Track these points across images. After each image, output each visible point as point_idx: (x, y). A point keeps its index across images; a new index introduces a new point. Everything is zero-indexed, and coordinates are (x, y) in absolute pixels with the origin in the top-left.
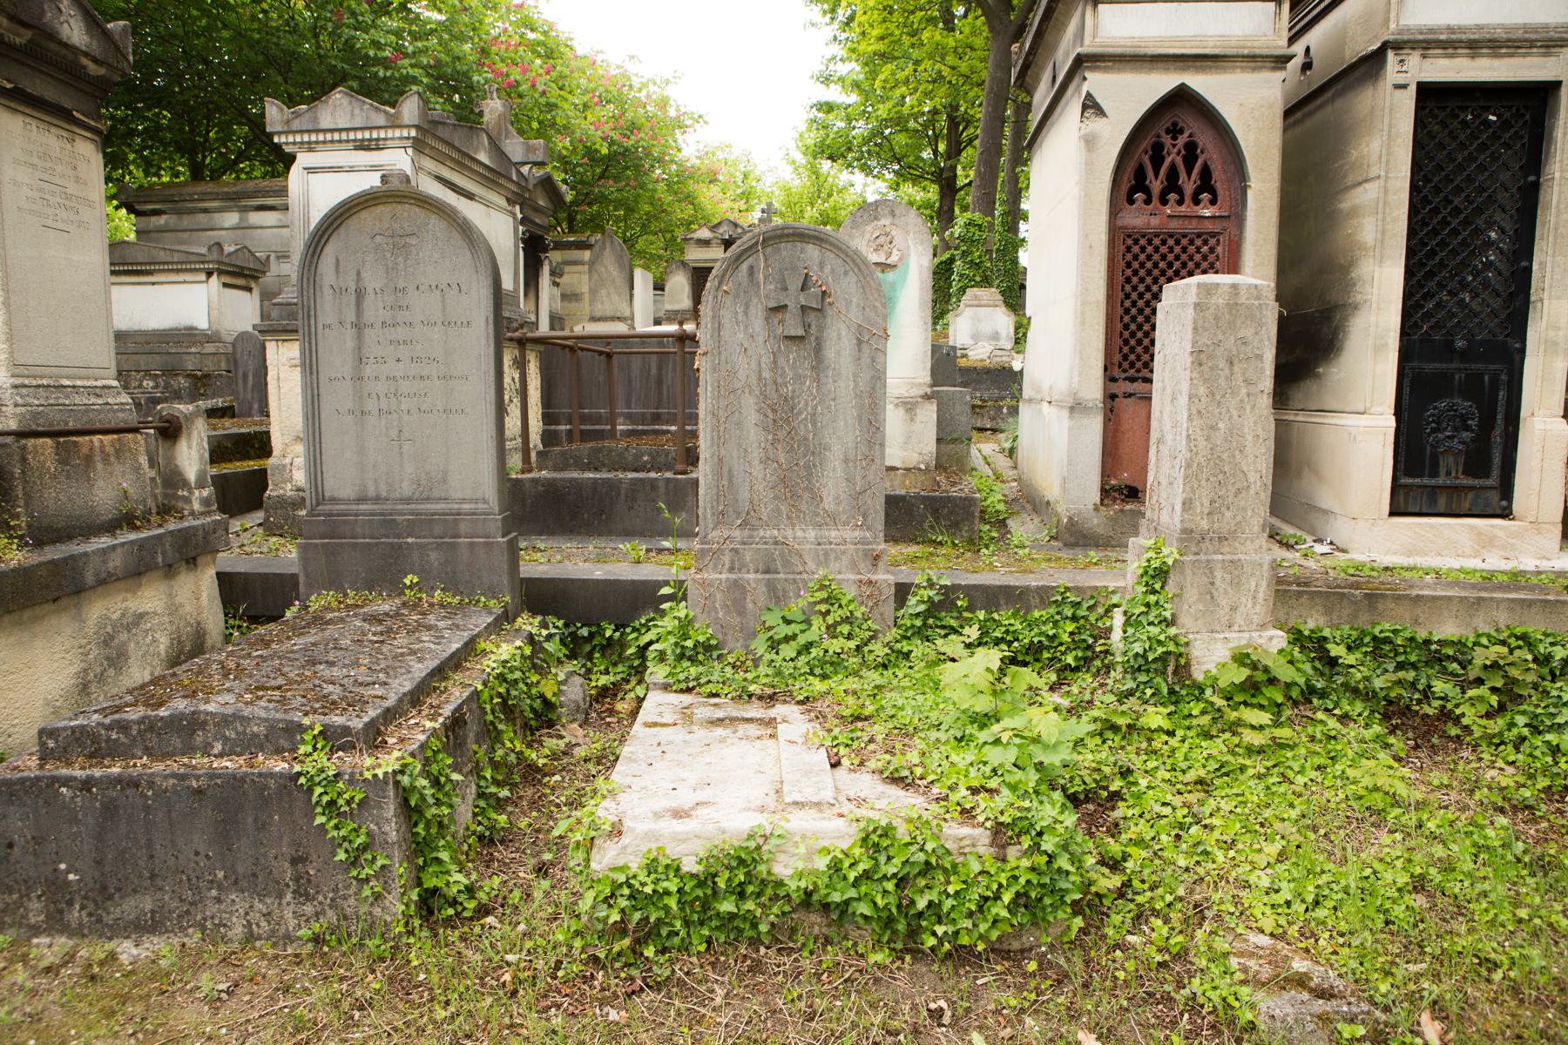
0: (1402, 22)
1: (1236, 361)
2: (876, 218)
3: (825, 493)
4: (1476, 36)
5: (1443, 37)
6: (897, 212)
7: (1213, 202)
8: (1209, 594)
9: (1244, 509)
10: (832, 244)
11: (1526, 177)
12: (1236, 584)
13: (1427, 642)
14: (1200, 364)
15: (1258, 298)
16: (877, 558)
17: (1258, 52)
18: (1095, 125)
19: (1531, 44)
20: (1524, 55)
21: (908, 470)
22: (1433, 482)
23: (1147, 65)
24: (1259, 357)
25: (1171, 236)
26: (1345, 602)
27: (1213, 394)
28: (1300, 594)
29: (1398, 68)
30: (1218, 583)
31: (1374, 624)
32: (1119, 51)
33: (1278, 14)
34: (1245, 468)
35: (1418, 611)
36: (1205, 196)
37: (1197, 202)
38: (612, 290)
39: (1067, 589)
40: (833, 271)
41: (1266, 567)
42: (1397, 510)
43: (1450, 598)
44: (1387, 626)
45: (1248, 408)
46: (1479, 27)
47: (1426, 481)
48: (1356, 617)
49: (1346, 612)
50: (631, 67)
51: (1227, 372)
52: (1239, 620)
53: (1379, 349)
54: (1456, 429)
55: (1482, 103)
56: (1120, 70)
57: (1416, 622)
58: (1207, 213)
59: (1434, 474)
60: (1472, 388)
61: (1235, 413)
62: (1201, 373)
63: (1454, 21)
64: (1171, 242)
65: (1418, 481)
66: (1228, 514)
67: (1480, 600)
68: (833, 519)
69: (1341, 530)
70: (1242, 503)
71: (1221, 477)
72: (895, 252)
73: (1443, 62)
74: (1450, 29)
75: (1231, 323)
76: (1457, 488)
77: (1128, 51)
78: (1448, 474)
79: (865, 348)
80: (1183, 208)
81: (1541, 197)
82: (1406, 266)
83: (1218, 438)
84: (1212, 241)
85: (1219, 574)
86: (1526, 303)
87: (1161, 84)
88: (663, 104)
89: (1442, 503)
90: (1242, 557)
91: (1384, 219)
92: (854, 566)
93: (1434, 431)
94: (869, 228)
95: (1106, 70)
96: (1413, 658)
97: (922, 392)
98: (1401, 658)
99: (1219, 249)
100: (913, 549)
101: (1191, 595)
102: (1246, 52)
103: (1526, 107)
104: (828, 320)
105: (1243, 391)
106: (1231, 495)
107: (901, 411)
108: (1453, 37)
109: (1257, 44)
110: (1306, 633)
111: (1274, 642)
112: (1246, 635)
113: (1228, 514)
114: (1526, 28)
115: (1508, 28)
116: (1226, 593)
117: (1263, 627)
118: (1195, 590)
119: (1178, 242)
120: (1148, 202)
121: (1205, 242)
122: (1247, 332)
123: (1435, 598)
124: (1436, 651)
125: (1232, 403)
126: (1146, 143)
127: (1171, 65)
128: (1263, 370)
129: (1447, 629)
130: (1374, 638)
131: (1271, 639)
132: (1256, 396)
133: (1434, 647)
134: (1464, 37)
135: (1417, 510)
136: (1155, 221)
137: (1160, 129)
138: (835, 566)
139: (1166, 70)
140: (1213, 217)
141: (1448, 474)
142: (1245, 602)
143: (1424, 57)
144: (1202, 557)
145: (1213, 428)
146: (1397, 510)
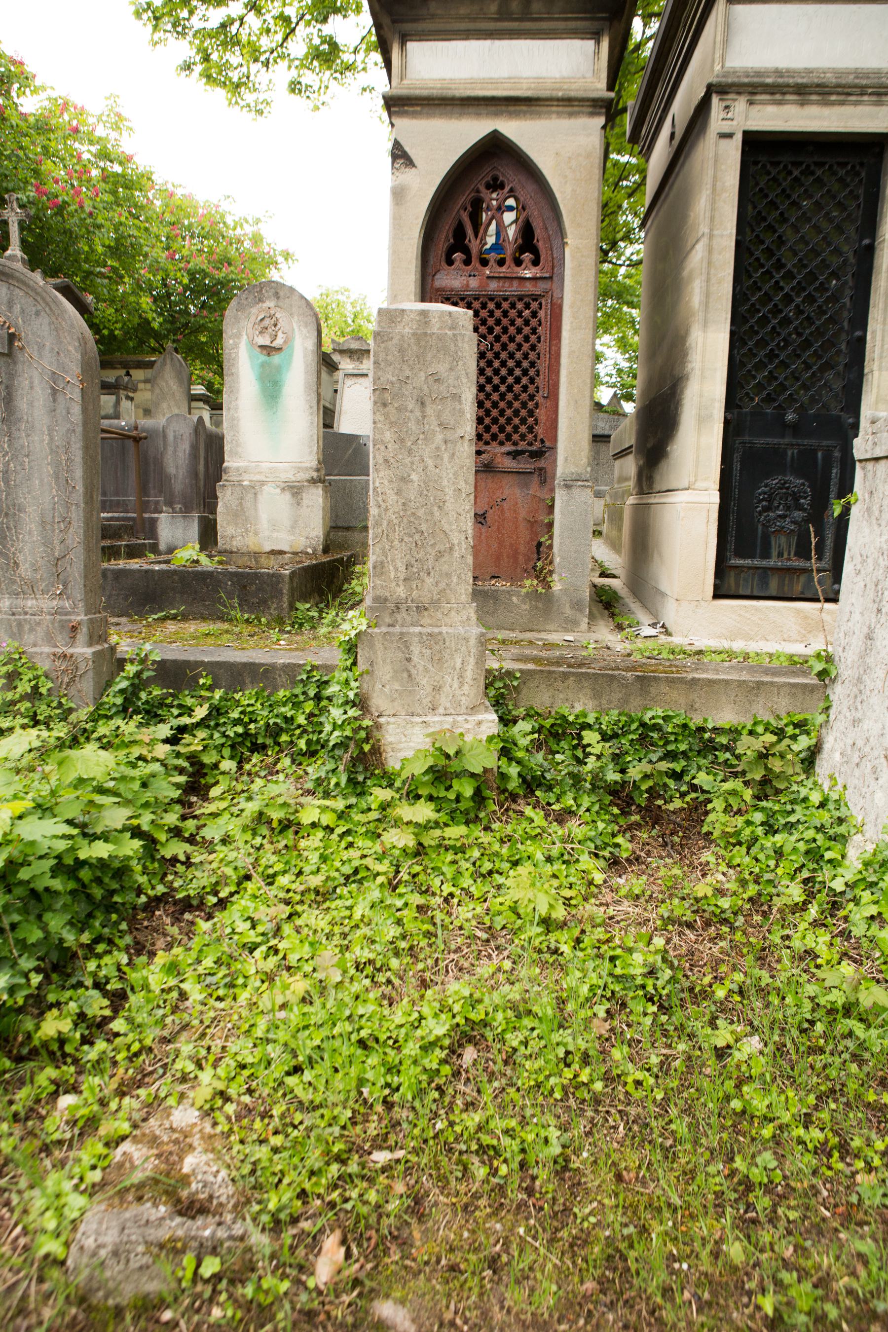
0: (729, 64)
1: (428, 402)
2: (261, 300)
3: (21, 558)
4: (805, 81)
5: (769, 80)
6: (281, 294)
7: (536, 262)
8: (405, 669)
9: (448, 575)
10: (19, 280)
11: (861, 240)
12: (438, 660)
13: (701, 730)
14: (385, 405)
15: (452, 328)
16: (74, 629)
17: (573, 94)
18: (408, 176)
19: (862, 90)
20: (856, 103)
21: (295, 554)
22: (765, 563)
23: (457, 109)
24: (456, 397)
25: (492, 299)
26: (615, 685)
27: (402, 441)
28: (566, 676)
29: (722, 115)
30: (415, 659)
31: (646, 708)
32: (425, 93)
33: (597, 53)
34: (446, 527)
35: (694, 696)
36: (527, 256)
37: (518, 262)
38: (172, 403)
39: (314, 668)
40: (23, 311)
41: (473, 642)
42: (719, 594)
43: (727, 682)
44: (660, 712)
45: (446, 457)
46: (809, 71)
47: (757, 562)
48: (626, 702)
49: (616, 696)
50: (225, 206)
51: (418, 414)
52: (444, 701)
53: (702, 420)
54: (788, 508)
55: (816, 159)
56: (429, 116)
57: (692, 707)
58: (528, 274)
59: (766, 555)
60: (806, 465)
61: (430, 462)
62: (387, 416)
63: (783, 63)
64: (491, 306)
65: (748, 562)
66: (429, 581)
67: (759, 684)
68: (31, 588)
69: (671, 613)
70: (445, 568)
71: (417, 537)
72: (280, 334)
73: (771, 109)
74: (778, 72)
75: (420, 357)
76: (788, 570)
77: (435, 93)
78: (780, 555)
79: (60, 398)
80: (503, 269)
81: (876, 263)
82: (732, 334)
83: (412, 493)
84: (534, 305)
85: (416, 649)
86: (860, 376)
87: (470, 131)
88: (257, 240)
89: (773, 586)
90: (444, 630)
91: (708, 280)
92: (50, 639)
93: (766, 509)
94: (254, 310)
95: (414, 115)
96: (683, 747)
97: (308, 477)
98: (671, 747)
99: (541, 314)
100: (205, 627)
101: (384, 672)
102: (560, 94)
103: (862, 164)
104: (19, 367)
105: (439, 438)
106: (431, 558)
107: (287, 496)
108: (780, 80)
109: (573, 87)
110: (571, 718)
111: (483, 727)
112: (450, 719)
113: (429, 581)
114: (857, 73)
115: (837, 73)
116: (426, 670)
117: (473, 709)
118: (388, 668)
119: (498, 306)
120: (467, 262)
121: (527, 306)
122: (441, 368)
123: (711, 682)
124: (711, 740)
125: (426, 451)
126: (464, 199)
127: (482, 110)
128: (462, 412)
129: (724, 716)
130: (643, 725)
131: (479, 723)
132: (454, 442)
133: (707, 736)
134: (791, 81)
135: (748, 593)
136: (474, 283)
137: (479, 182)
138: (28, 638)
139: (478, 115)
140: (534, 279)
141: (780, 555)
142: (451, 683)
143: (751, 103)
144: (398, 629)
145: (405, 480)
146: (719, 594)
